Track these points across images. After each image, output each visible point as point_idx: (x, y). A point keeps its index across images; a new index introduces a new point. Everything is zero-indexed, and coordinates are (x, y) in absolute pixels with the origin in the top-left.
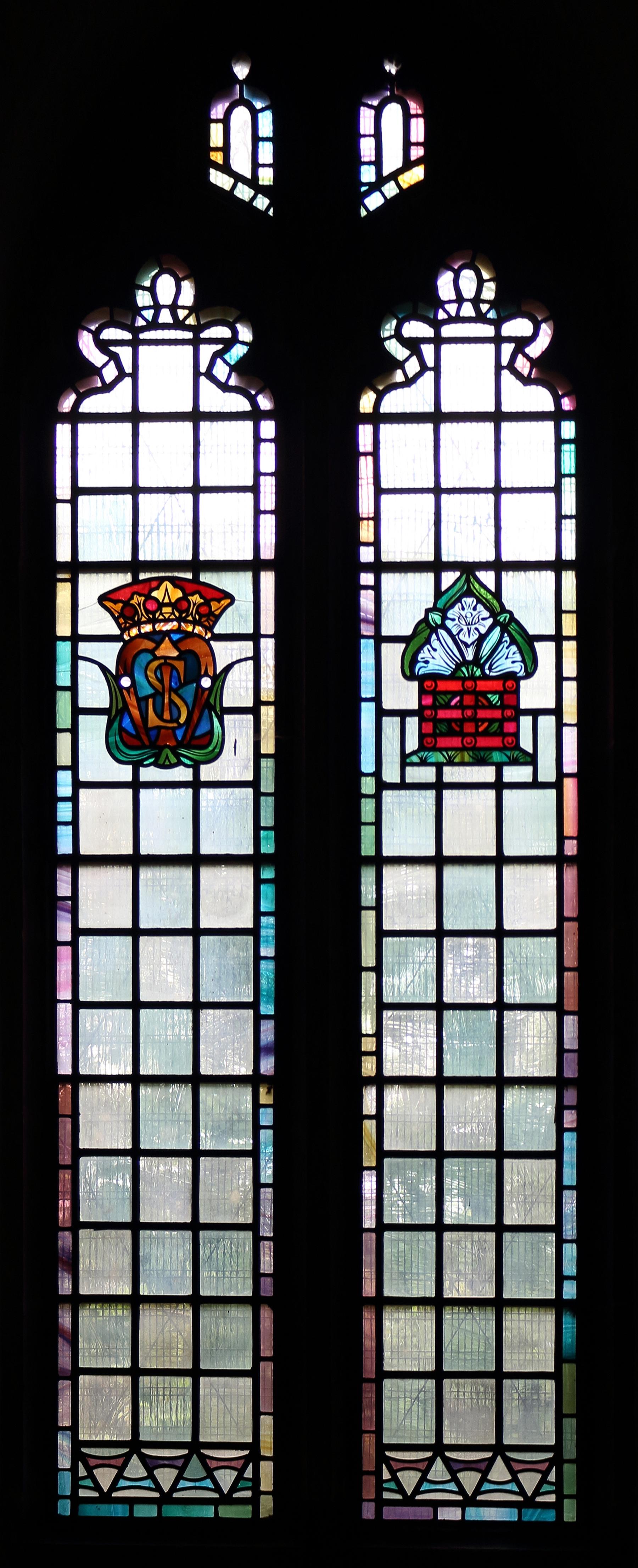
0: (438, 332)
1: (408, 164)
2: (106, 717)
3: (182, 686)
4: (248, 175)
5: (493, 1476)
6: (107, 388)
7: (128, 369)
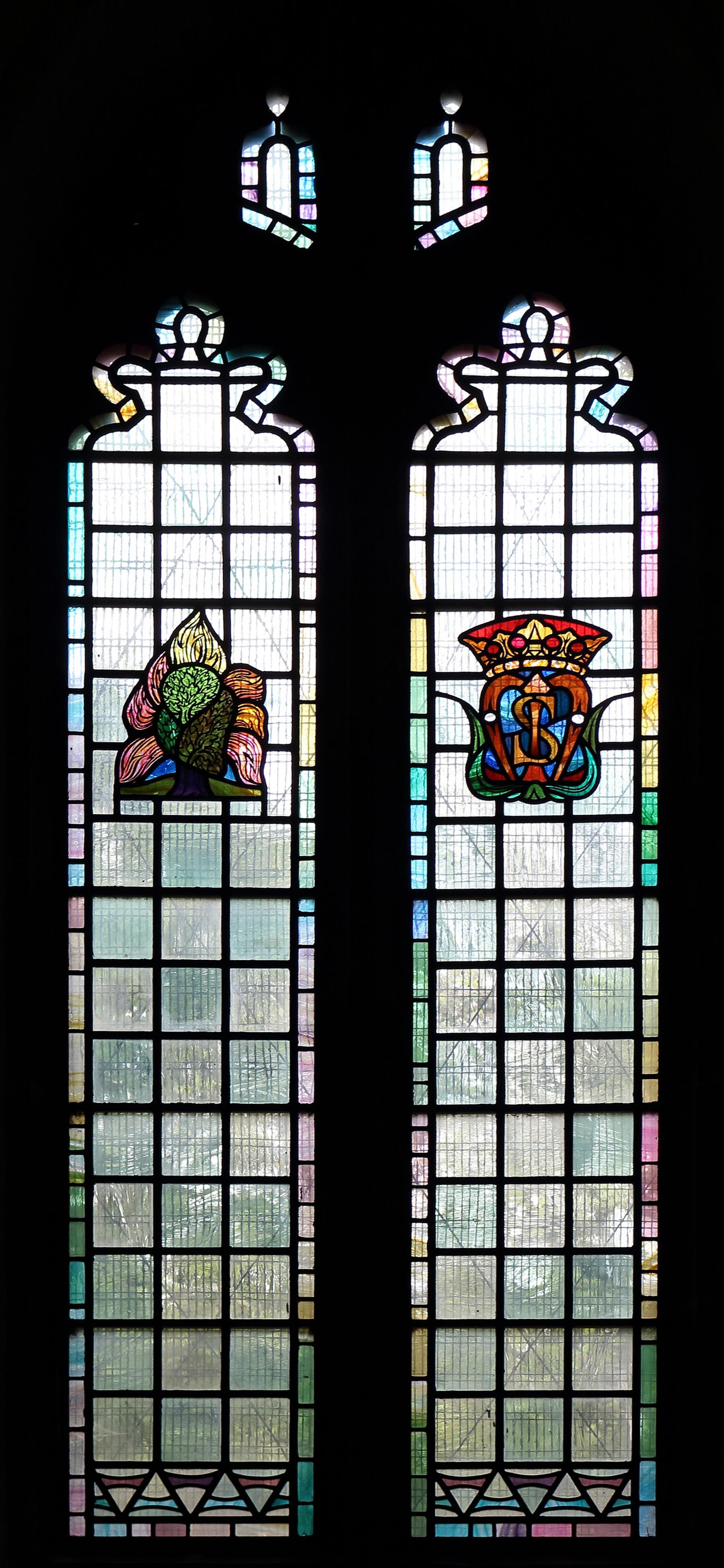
1: (469, 206)
2: (466, 755)
3: (552, 722)
4: (287, 212)
6: (467, 426)
7: (148, 405)
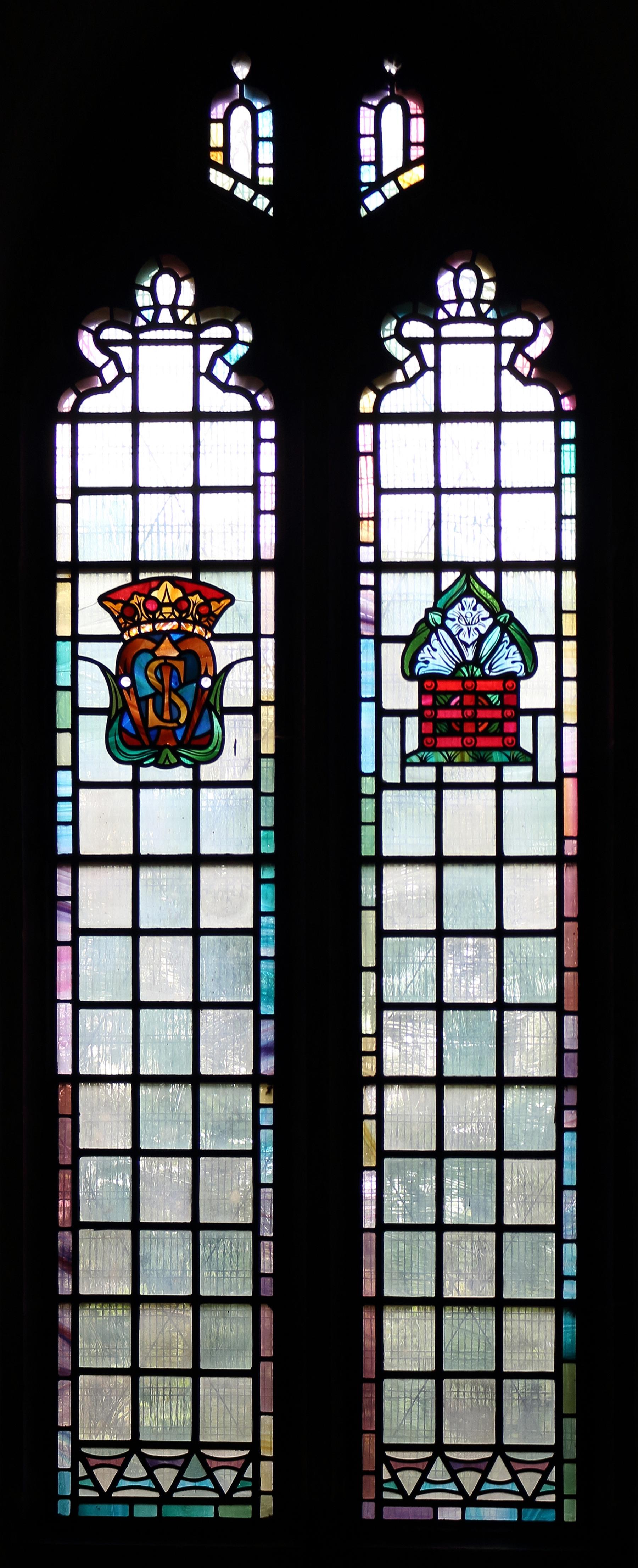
0: (438, 332)
1: (408, 164)
2: (106, 717)
3: (182, 686)
4: (248, 175)
5: (493, 1476)
6: (107, 388)
7: (128, 369)
